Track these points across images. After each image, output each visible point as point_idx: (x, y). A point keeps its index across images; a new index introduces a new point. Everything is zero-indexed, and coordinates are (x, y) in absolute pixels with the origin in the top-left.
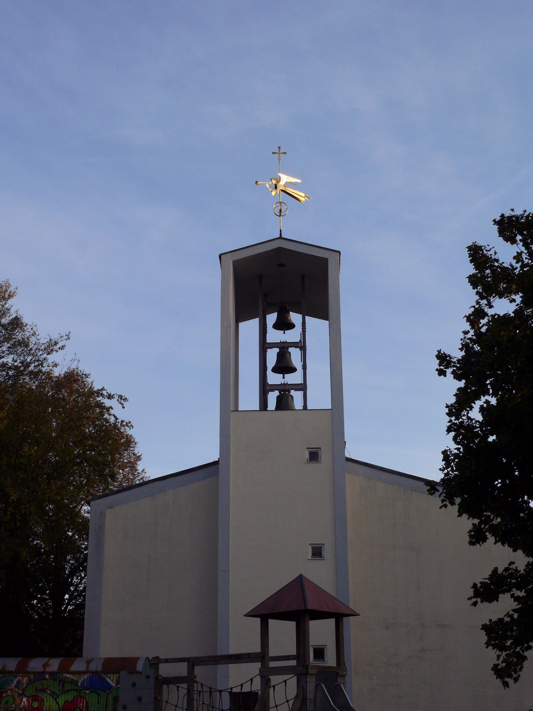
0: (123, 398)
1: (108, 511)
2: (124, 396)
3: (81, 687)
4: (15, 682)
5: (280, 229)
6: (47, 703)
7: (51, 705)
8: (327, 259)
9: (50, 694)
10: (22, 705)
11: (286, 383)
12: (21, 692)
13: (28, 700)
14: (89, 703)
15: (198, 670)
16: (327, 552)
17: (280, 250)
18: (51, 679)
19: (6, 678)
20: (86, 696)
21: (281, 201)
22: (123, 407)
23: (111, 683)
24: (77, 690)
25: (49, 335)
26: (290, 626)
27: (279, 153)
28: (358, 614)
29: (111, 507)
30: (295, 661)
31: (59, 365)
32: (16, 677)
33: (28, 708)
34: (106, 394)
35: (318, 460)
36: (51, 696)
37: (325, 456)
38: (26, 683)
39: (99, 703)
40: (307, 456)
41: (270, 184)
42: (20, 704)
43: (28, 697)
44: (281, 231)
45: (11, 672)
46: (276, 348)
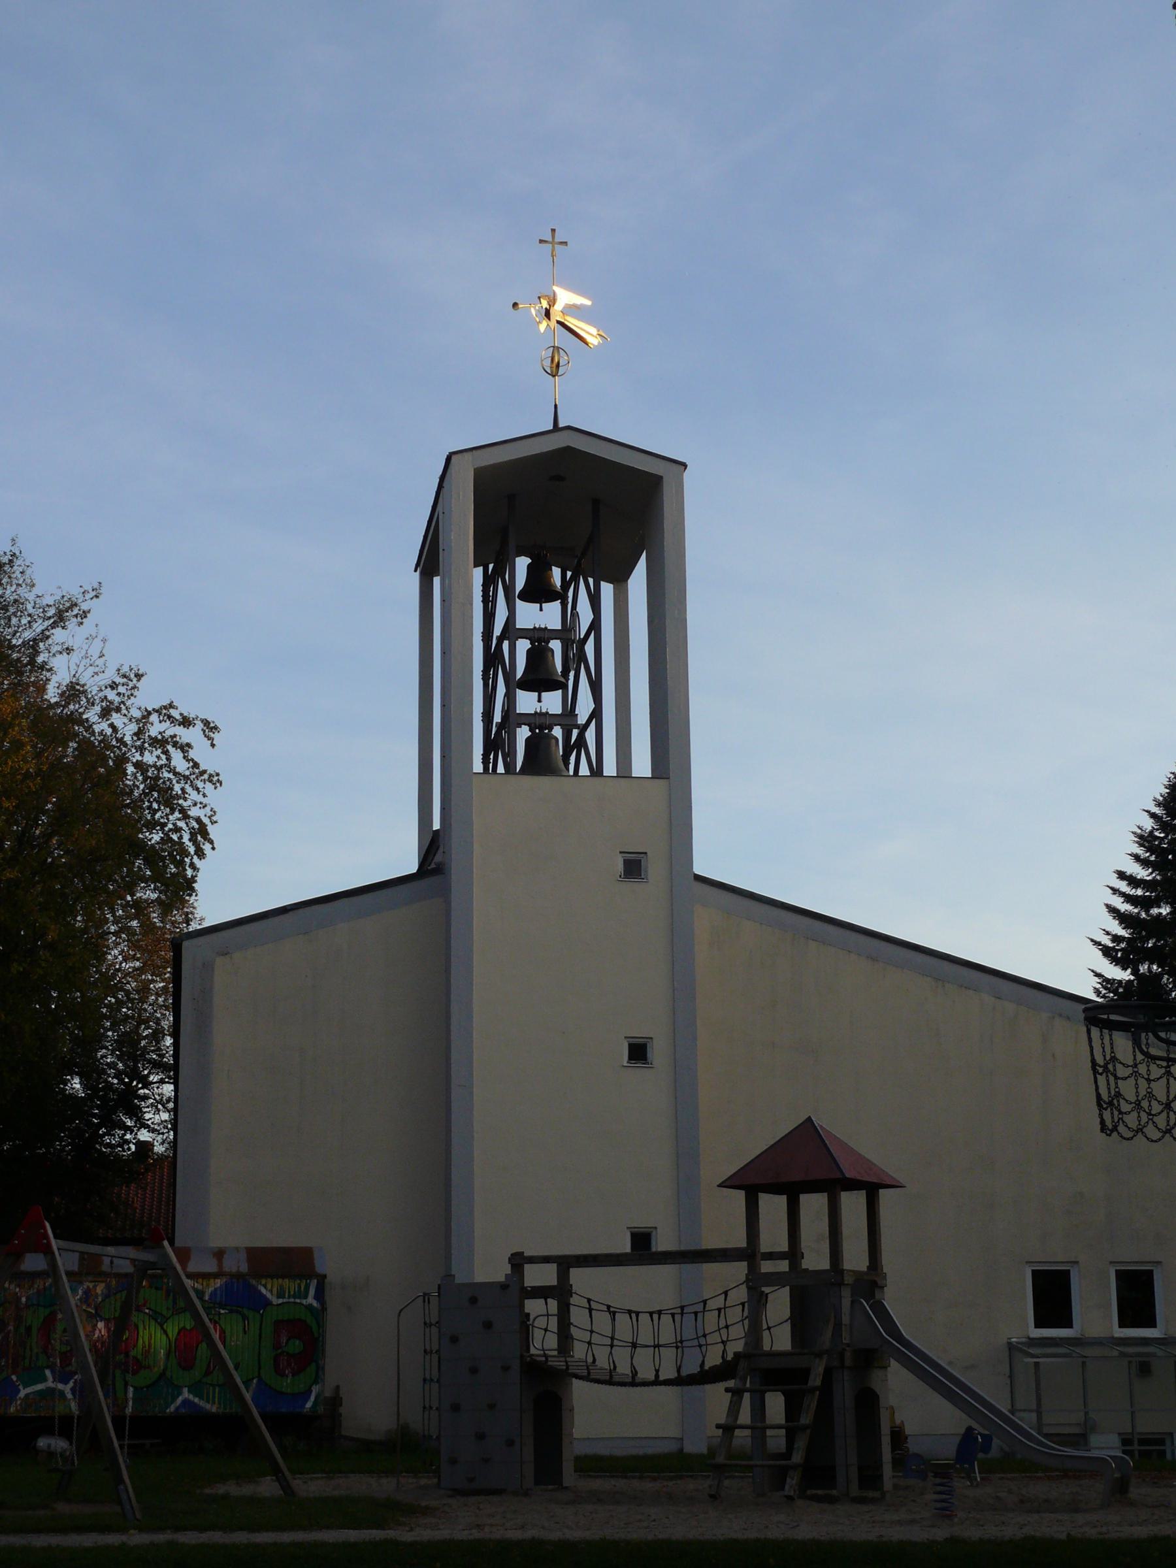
0: (212, 725)
1: (219, 961)
2: (213, 722)
3: (211, 1303)
5: (555, 403)
6: (145, 1331)
7: (153, 1336)
8: (661, 477)
9: (150, 1316)
10: (96, 1336)
11: (544, 711)
12: (93, 1312)
13: (108, 1325)
14: (227, 1332)
15: (579, 1277)
16: (658, 1053)
17: (567, 453)
18: (151, 1287)
20: (219, 1319)
21: (556, 345)
22: (213, 745)
23: (269, 1295)
25: (60, 588)
26: (781, 1201)
27: (553, 243)
28: (901, 1184)
30: (786, 1262)
31: (73, 650)
32: (81, 1283)
33: (107, 1340)
34: (178, 717)
35: (641, 876)
36: (153, 1318)
37: (655, 869)
38: (102, 1293)
39: (245, 1332)
40: (620, 867)
41: (537, 308)
42: (92, 1334)
44: (556, 406)
46: (524, 640)
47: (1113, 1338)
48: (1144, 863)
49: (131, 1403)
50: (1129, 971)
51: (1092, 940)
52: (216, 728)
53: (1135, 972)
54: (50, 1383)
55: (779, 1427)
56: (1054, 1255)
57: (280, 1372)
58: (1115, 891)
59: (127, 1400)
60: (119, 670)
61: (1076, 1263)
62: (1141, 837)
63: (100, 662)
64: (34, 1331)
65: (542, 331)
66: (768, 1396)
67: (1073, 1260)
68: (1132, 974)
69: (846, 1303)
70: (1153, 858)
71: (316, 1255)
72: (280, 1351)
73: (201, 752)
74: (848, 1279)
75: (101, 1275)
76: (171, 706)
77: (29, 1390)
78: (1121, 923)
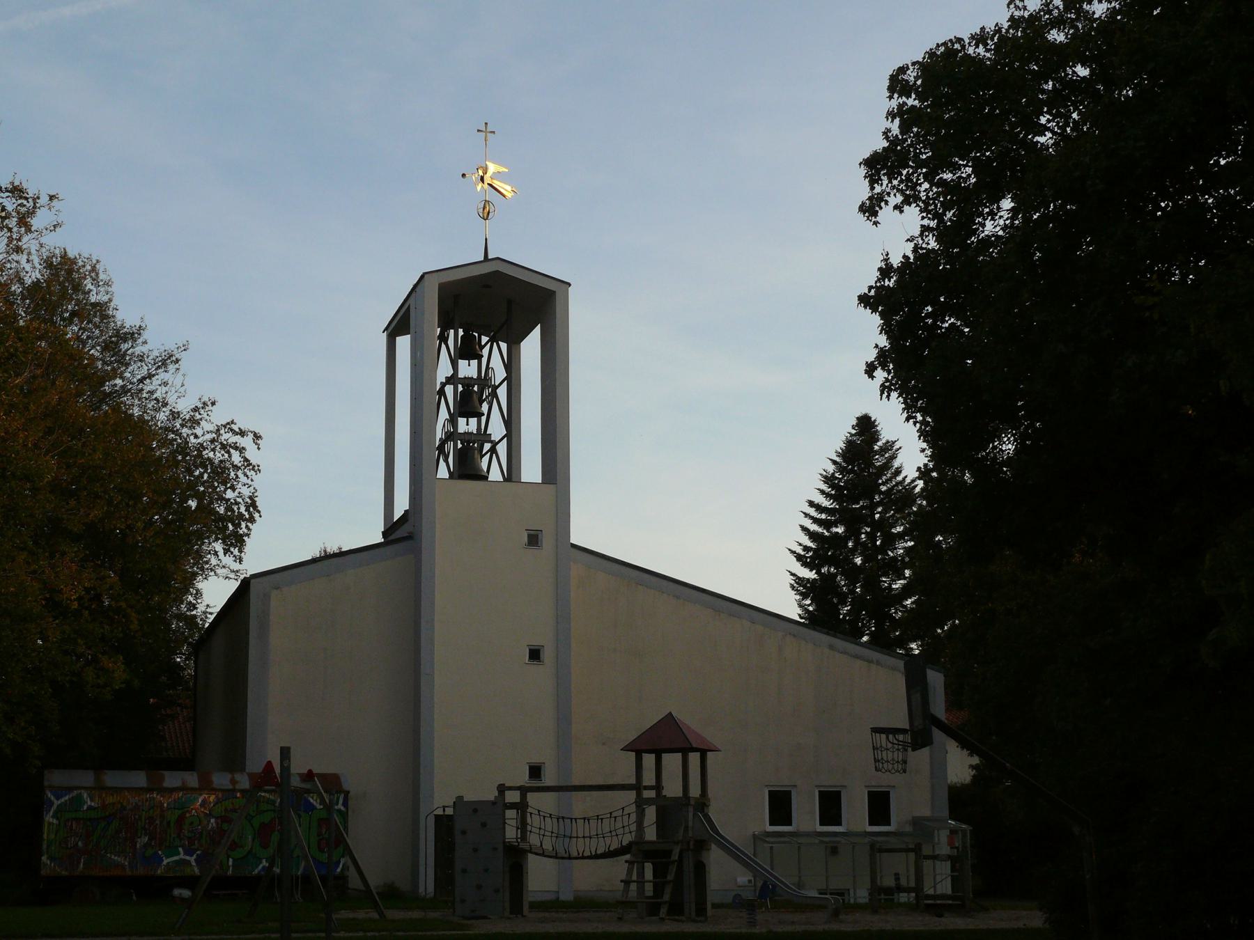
1: (274, 593)
4: (200, 801)
8: (555, 292)
12: (208, 812)
16: (547, 655)
19: (189, 795)
22: (259, 449)
23: (315, 803)
24: (274, 811)
27: (486, 132)
29: (277, 588)
32: (201, 795)
34: (237, 430)
37: (547, 541)
40: (526, 539)
43: (217, 818)
44: (486, 239)
45: (193, 789)
47: (816, 832)
48: (827, 495)
49: (231, 868)
50: (814, 571)
51: (790, 550)
52: (260, 437)
53: (818, 573)
54: (182, 856)
55: (650, 882)
56: (782, 781)
57: (321, 850)
58: (806, 515)
59: (229, 867)
60: (200, 399)
61: (795, 786)
62: (826, 477)
63: (182, 390)
64: (172, 825)
65: (479, 190)
66: (646, 864)
67: (793, 784)
68: (816, 573)
69: (691, 815)
70: (833, 492)
71: (342, 779)
72: (321, 837)
73: (252, 454)
74: (692, 802)
75: (213, 790)
76: (232, 422)
77: (169, 860)
78: (810, 538)
